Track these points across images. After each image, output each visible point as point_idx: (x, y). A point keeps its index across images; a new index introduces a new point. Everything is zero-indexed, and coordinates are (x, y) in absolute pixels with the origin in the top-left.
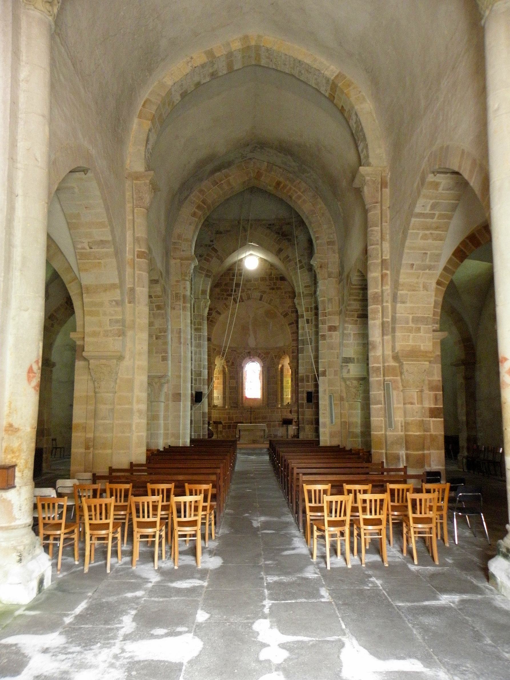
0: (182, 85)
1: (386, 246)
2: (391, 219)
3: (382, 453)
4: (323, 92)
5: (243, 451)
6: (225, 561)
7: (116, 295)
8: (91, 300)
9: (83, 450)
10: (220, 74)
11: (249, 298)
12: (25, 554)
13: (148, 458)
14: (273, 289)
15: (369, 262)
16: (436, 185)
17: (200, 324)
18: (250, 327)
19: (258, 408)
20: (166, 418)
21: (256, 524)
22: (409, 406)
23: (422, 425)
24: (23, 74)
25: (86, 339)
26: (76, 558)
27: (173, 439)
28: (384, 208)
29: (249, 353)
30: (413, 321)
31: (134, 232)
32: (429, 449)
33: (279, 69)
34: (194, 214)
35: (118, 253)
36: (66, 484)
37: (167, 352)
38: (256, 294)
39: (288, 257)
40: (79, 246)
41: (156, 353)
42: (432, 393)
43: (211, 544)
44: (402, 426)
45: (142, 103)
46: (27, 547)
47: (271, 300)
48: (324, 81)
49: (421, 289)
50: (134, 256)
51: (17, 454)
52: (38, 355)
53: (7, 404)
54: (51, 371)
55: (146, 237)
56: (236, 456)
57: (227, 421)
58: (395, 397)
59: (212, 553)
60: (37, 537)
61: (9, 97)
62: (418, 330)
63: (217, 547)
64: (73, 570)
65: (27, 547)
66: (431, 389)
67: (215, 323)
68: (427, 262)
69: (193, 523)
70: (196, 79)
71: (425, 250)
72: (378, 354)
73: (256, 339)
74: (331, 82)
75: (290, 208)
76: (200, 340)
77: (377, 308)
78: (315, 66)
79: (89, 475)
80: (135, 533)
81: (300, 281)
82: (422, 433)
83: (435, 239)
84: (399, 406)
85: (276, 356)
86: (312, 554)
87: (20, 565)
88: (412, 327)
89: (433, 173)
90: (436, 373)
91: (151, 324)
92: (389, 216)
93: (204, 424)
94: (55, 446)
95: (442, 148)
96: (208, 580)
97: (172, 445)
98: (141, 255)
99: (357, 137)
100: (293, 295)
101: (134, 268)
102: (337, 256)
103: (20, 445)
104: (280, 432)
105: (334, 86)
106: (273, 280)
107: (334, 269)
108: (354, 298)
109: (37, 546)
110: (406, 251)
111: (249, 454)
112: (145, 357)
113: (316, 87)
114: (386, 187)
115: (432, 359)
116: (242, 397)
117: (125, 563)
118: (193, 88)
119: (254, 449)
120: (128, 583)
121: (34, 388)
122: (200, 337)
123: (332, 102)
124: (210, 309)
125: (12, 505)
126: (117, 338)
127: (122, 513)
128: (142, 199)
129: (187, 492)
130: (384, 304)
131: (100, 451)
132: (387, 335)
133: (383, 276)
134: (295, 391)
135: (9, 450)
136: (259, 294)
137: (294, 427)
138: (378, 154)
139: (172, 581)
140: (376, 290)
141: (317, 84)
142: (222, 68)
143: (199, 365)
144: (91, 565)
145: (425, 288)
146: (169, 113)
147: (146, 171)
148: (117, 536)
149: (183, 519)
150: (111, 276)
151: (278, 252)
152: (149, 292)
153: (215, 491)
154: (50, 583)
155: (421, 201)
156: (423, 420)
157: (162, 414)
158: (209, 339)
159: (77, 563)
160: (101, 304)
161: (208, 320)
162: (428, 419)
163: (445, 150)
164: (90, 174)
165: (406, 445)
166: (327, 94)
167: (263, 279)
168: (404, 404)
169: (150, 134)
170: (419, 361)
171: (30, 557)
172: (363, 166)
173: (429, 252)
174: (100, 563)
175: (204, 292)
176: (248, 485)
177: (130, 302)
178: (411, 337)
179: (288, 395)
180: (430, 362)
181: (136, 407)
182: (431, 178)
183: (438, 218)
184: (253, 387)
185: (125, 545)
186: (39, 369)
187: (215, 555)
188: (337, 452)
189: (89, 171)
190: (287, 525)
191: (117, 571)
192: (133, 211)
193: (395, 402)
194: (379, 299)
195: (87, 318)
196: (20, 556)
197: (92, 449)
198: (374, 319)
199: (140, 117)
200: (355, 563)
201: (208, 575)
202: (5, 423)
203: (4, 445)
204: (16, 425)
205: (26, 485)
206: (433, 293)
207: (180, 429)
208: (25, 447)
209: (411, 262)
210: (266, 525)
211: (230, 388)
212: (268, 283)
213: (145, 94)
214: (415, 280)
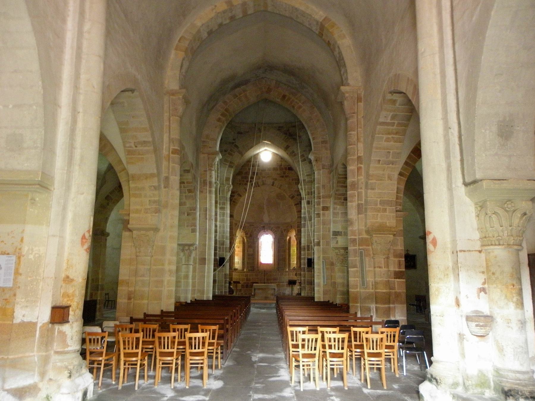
0: (208, 26)
1: (361, 146)
2: (365, 125)
3: (358, 306)
4: (315, 31)
5: (256, 306)
6: (225, 384)
7: (154, 182)
8: (136, 185)
9: (126, 301)
10: (237, 17)
11: (264, 184)
12: (74, 372)
13: (176, 308)
14: (283, 177)
15: (348, 158)
16: (394, 102)
17: (224, 204)
18: (265, 207)
19: (270, 271)
20: (194, 278)
21: (254, 359)
22: (377, 269)
23: (388, 284)
24: (87, 27)
25: (130, 215)
26: (114, 379)
27: (199, 294)
28: (359, 117)
29: (264, 227)
30: (380, 204)
31: (170, 135)
32: (393, 303)
33: (281, 13)
34: (219, 120)
35: (156, 150)
36: (109, 325)
37: (196, 226)
38: (269, 181)
39: (293, 152)
40: (128, 145)
41: (187, 226)
42: (396, 260)
43: (218, 372)
44: (372, 285)
45: (178, 39)
46: (75, 367)
47: (281, 185)
48: (315, 23)
49: (387, 179)
50: (169, 153)
51: (71, 298)
52: (90, 226)
53: (66, 261)
54: (106, 240)
55: (179, 138)
56: (249, 309)
57: (245, 281)
58: (367, 262)
59: (216, 378)
60: (84, 361)
61: (75, 44)
62: (385, 210)
63: (222, 374)
64: (111, 387)
65: (75, 367)
66: (396, 256)
67: (237, 203)
68: (390, 158)
69: (202, 354)
70: (219, 21)
71: (388, 149)
72: (354, 229)
73: (269, 216)
74: (319, 24)
75: (295, 116)
76: (224, 216)
77: (354, 193)
78: (307, 12)
79: (128, 319)
80: (158, 361)
81: (302, 171)
82: (388, 291)
83: (395, 142)
84: (371, 269)
85: (285, 230)
86: (291, 380)
87: (69, 380)
88: (380, 208)
89: (391, 93)
90: (399, 244)
91: (181, 204)
92: (362, 123)
93: (225, 283)
94: (107, 299)
95: (396, 75)
96: (209, 395)
97: (197, 299)
98: (174, 152)
99: (340, 63)
100: (297, 181)
101: (169, 162)
102: (329, 152)
103: (74, 291)
104: (287, 291)
105: (322, 27)
106: (284, 170)
107: (327, 163)
108: (341, 185)
109: (83, 367)
110: (374, 150)
111: (261, 308)
112: (176, 229)
113: (309, 27)
114: (361, 102)
115: (395, 233)
116: (258, 262)
117: (150, 384)
118: (217, 27)
119: (265, 304)
120: (149, 397)
121: (86, 250)
122: (224, 214)
123: (321, 37)
124: (233, 192)
125: (66, 336)
126: (154, 214)
127: (151, 346)
128: (176, 110)
129: (200, 330)
130: (359, 190)
131: (139, 302)
132: (361, 214)
133: (359, 169)
134: (299, 258)
135: (66, 295)
136: (272, 181)
137: (298, 287)
138: (355, 76)
139: (182, 396)
140: (354, 180)
141: (310, 24)
142: (239, 14)
143: (223, 237)
144: (124, 385)
145: (390, 178)
146: (197, 48)
147: (180, 89)
148: (144, 362)
149: (194, 351)
150: (150, 167)
151: (286, 148)
152: (180, 179)
153: (222, 332)
154: (92, 396)
155: (384, 113)
156: (389, 281)
157: (191, 276)
158: (231, 216)
159: (114, 383)
160: (143, 189)
161: (231, 200)
162: (393, 280)
163: (397, 77)
164: (136, 93)
165: (376, 299)
166: (317, 33)
167: (274, 169)
168: (375, 268)
169: (184, 62)
170: (385, 234)
171: (78, 375)
172: (345, 86)
173: (391, 151)
174: (131, 383)
175: (227, 179)
176: (255, 331)
177: (165, 187)
178: (379, 215)
179: (294, 262)
180: (394, 235)
181: (167, 267)
182: (389, 97)
183: (397, 126)
184: (266, 253)
185: (152, 371)
186: (90, 236)
187: (219, 379)
188: (327, 307)
189: (136, 91)
190: (279, 360)
191: (143, 389)
192: (170, 119)
193: (367, 266)
194: (354, 186)
195: (133, 199)
196: (70, 373)
197: (132, 300)
198: (351, 202)
199: (176, 49)
200: (323, 387)
201: (210, 393)
202: (63, 276)
203: (62, 291)
204: (71, 277)
205: (77, 321)
206: (396, 183)
207: (204, 285)
208: (77, 293)
209: (378, 159)
210: (262, 360)
211: (249, 255)
212: (279, 172)
213: (181, 32)
214: (381, 172)
